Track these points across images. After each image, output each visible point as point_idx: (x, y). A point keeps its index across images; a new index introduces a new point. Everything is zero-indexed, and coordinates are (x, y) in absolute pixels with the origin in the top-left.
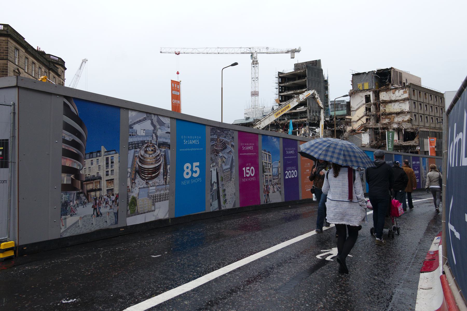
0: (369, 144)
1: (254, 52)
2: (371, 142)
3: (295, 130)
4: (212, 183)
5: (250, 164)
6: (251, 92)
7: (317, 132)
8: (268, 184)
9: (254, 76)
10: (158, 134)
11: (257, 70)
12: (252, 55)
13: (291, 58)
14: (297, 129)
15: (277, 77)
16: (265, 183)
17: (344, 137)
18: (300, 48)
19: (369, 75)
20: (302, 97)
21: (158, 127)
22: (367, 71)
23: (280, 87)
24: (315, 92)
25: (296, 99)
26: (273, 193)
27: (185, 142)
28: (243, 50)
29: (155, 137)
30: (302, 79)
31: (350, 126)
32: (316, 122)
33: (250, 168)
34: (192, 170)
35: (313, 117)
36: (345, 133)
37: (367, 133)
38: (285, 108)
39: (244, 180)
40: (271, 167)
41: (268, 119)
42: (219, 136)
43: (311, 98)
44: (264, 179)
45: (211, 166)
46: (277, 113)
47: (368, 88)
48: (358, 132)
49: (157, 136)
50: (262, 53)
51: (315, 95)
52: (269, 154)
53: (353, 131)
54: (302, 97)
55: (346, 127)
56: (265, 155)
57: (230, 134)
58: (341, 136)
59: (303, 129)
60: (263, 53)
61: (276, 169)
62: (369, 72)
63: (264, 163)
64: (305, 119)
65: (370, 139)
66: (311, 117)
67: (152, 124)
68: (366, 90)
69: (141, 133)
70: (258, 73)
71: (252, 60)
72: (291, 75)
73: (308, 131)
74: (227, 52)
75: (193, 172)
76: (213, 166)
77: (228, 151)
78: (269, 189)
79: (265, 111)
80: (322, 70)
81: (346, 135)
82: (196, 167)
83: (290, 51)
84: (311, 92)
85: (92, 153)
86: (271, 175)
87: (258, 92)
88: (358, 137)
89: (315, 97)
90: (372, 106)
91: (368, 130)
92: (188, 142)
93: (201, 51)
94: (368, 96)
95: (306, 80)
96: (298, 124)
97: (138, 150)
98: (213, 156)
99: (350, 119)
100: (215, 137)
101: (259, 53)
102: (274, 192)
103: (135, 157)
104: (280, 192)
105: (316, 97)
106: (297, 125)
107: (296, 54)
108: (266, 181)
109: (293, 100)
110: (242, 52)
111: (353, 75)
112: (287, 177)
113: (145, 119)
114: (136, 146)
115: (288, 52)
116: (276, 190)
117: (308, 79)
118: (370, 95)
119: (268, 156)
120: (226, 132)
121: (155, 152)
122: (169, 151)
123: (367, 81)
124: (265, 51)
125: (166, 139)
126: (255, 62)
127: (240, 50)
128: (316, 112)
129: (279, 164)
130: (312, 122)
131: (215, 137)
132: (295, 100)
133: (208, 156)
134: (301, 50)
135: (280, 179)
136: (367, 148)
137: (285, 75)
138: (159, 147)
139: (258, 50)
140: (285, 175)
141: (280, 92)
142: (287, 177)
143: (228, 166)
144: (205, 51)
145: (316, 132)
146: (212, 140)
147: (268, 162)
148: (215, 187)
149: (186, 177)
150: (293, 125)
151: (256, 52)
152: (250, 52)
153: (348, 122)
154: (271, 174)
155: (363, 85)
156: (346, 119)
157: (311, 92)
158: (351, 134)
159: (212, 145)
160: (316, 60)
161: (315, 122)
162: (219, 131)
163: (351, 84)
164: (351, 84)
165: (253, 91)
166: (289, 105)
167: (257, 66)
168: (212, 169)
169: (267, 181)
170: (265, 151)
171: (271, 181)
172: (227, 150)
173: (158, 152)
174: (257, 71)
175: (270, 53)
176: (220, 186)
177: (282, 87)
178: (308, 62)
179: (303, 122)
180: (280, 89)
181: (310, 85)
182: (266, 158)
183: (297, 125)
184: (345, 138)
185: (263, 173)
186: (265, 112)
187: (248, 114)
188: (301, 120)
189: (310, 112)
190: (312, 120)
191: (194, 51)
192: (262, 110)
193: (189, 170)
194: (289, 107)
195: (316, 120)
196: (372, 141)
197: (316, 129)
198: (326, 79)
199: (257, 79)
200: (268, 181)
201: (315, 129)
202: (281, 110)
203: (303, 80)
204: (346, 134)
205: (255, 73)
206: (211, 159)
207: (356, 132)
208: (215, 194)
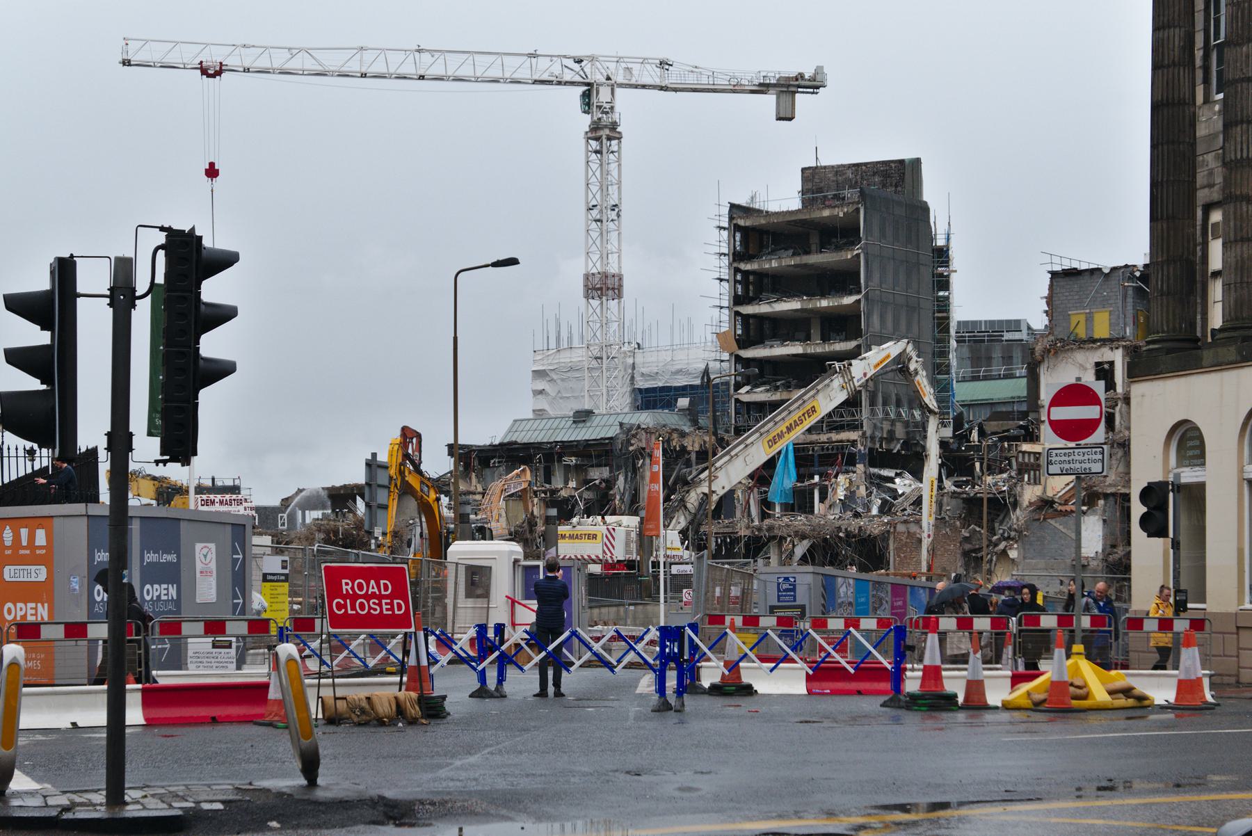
0: (1101, 557)
1: (600, 78)
2: (1109, 550)
3: (807, 483)
6: (587, 277)
7: (900, 492)
9: (598, 196)
11: (613, 167)
12: (587, 97)
13: (779, 119)
14: (817, 478)
15: (726, 225)
17: (1010, 528)
18: (819, 70)
19: (1113, 282)
20: (861, 369)
22: (1107, 263)
23: (739, 277)
24: (910, 347)
25: (841, 380)
28: (544, 69)
30: (838, 248)
31: (1036, 481)
32: (898, 447)
35: (886, 426)
36: (1014, 509)
37: (1095, 513)
38: (800, 414)
41: (741, 458)
43: (892, 370)
46: (770, 437)
47: (1106, 335)
48: (1063, 508)
50: (636, 87)
51: (910, 359)
53: (1045, 504)
54: (861, 369)
55: (1019, 488)
58: (1001, 523)
59: (841, 478)
60: (644, 87)
62: (1114, 269)
64: (853, 435)
65: (1105, 538)
66: (875, 426)
68: (1100, 340)
70: (619, 183)
71: (587, 119)
72: (789, 222)
73: (862, 491)
74: (466, 71)
79: (641, 369)
80: (925, 209)
81: (1018, 519)
82: (31, 608)
83: (774, 85)
84: (892, 349)
87: (620, 279)
88: (1061, 528)
89: (908, 368)
90: (1118, 409)
91: (1101, 502)
93: (332, 61)
94: (1106, 366)
95: (858, 255)
96: (819, 455)
99: (1035, 453)
101: (621, 85)
105: (912, 366)
106: (816, 460)
107: (802, 100)
109: (827, 381)
110: (536, 77)
111: (1054, 274)
115: (763, 88)
117: (866, 254)
118: (1112, 363)
123: (1104, 303)
124: (651, 75)
126: (607, 131)
127: (528, 64)
128: (899, 404)
130: (881, 446)
132: (837, 381)
134: (829, 83)
136: (1095, 571)
137: (763, 221)
139: (621, 71)
141: (738, 300)
144: (354, 67)
145: (894, 494)
150: (797, 458)
151: (608, 78)
152: (578, 79)
153: (1027, 465)
155: (1089, 319)
156: (1020, 455)
157: (892, 349)
158: (1037, 517)
160: (901, 162)
161: (892, 446)
163: (1046, 312)
164: (1046, 312)
165: (594, 271)
166: (815, 404)
167: (615, 148)
174: (615, 173)
175: (676, 90)
177: (746, 274)
178: (866, 164)
179: (841, 447)
180: (736, 281)
181: (876, 277)
183: (816, 460)
184: (1015, 530)
186: (644, 370)
187: (555, 377)
188: (835, 436)
189: (873, 403)
190: (882, 439)
191: (293, 65)
192: (630, 361)
194: (813, 410)
195: (898, 440)
196: (1114, 546)
197: (897, 480)
198: (940, 242)
199: (613, 215)
201: (891, 480)
202: (787, 424)
203: (843, 253)
204: (1018, 517)
205: (604, 188)
207: (1056, 510)
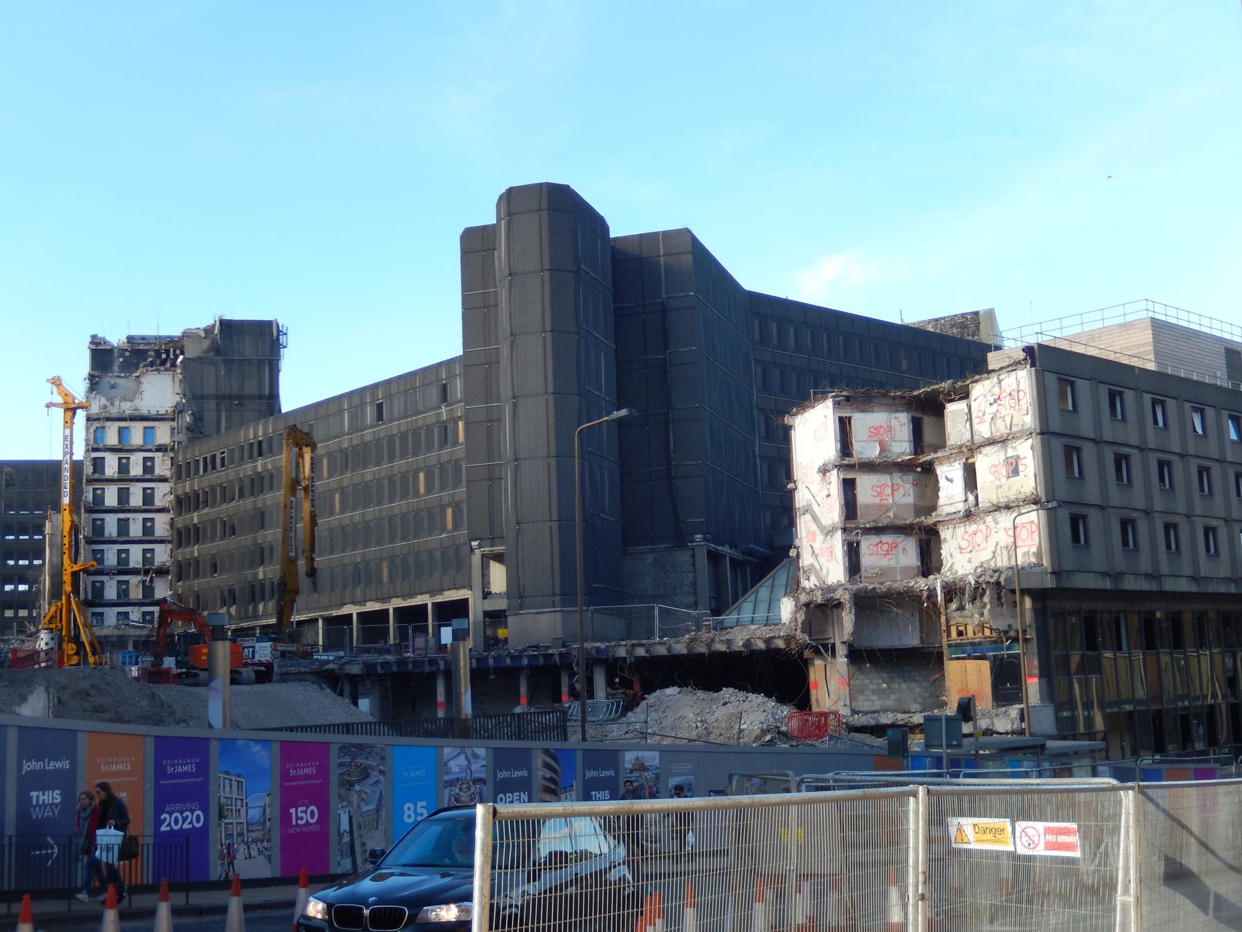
4: (342, 832)
5: (306, 801)
8: (233, 841)
10: (473, 769)
16: (223, 839)
21: (472, 760)
26: (246, 859)
27: (170, 770)
29: (469, 773)
33: (307, 808)
34: (415, 811)
39: (292, 831)
40: (242, 806)
42: (353, 758)
44: (221, 832)
45: (340, 806)
49: (471, 771)
52: (238, 779)
56: (227, 782)
57: (376, 753)
61: (258, 809)
63: (222, 798)
67: (467, 758)
69: (455, 769)
75: (416, 814)
76: (342, 807)
77: (372, 782)
78: (236, 851)
82: (421, 807)
85: (566, 788)
86: (243, 823)
92: (174, 770)
97: (453, 788)
98: (342, 791)
100: (347, 759)
102: (250, 857)
103: (450, 795)
104: (269, 859)
108: (226, 835)
112: (164, 828)
113: (459, 754)
114: (451, 783)
116: (254, 853)
119: (234, 784)
120: (368, 750)
121: (470, 789)
122: (485, 788)
125: (481, 773)
129: (268, 799)
131: (347, 759)
133: (334, 790)
135: (269, 830)
138: (474, 784)
140: (158, 822)
142: (164, 828)
143: (373, 807)
146: (341, 765)
147: (234, 796)
148: (346, 839)
149: (407, 820)
154: (244, 820)
159: (340, 774)
160: (976, 313)
162: (354, 750)
168: (341, 812)
169: (229, 835)
170: (227, 773)
171: (240, 835)
172: (371, 781)
173: (473, 789)
176: (356, 836)
182: (231, 788)
185: (220, 819)
193: (411, 812)
200: (232, 834)
206: (340, 796)
208: (347, 850)
